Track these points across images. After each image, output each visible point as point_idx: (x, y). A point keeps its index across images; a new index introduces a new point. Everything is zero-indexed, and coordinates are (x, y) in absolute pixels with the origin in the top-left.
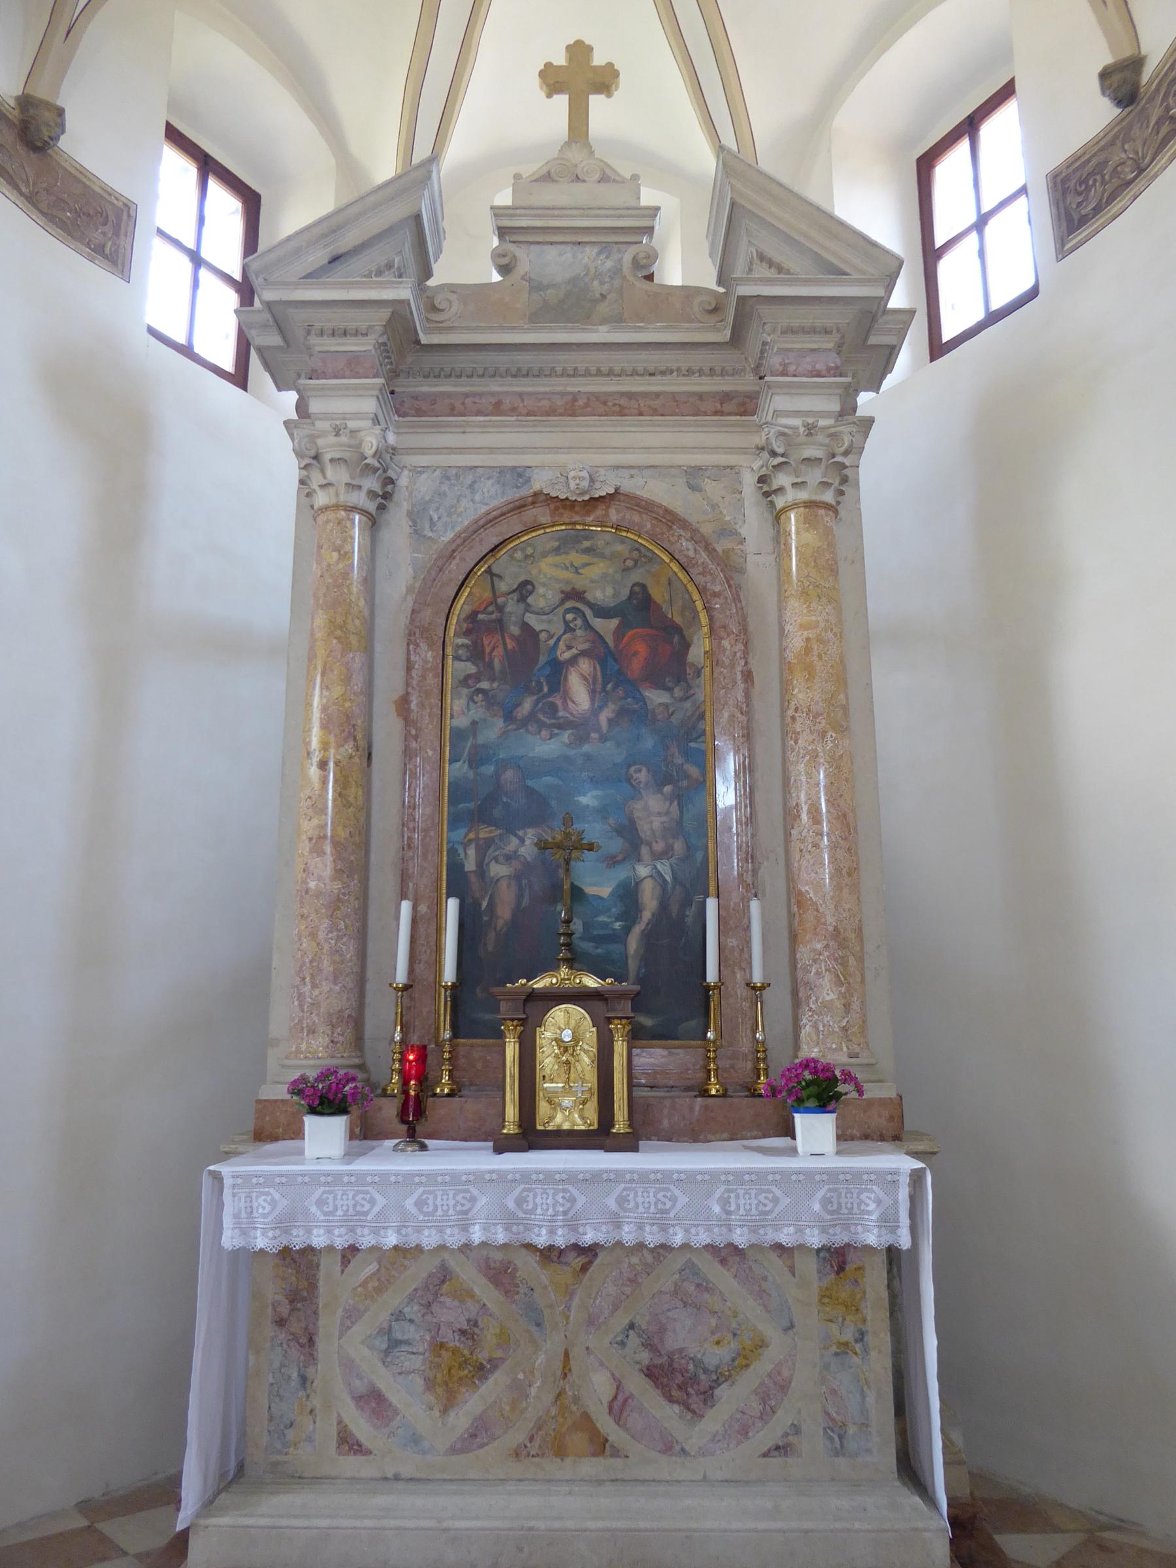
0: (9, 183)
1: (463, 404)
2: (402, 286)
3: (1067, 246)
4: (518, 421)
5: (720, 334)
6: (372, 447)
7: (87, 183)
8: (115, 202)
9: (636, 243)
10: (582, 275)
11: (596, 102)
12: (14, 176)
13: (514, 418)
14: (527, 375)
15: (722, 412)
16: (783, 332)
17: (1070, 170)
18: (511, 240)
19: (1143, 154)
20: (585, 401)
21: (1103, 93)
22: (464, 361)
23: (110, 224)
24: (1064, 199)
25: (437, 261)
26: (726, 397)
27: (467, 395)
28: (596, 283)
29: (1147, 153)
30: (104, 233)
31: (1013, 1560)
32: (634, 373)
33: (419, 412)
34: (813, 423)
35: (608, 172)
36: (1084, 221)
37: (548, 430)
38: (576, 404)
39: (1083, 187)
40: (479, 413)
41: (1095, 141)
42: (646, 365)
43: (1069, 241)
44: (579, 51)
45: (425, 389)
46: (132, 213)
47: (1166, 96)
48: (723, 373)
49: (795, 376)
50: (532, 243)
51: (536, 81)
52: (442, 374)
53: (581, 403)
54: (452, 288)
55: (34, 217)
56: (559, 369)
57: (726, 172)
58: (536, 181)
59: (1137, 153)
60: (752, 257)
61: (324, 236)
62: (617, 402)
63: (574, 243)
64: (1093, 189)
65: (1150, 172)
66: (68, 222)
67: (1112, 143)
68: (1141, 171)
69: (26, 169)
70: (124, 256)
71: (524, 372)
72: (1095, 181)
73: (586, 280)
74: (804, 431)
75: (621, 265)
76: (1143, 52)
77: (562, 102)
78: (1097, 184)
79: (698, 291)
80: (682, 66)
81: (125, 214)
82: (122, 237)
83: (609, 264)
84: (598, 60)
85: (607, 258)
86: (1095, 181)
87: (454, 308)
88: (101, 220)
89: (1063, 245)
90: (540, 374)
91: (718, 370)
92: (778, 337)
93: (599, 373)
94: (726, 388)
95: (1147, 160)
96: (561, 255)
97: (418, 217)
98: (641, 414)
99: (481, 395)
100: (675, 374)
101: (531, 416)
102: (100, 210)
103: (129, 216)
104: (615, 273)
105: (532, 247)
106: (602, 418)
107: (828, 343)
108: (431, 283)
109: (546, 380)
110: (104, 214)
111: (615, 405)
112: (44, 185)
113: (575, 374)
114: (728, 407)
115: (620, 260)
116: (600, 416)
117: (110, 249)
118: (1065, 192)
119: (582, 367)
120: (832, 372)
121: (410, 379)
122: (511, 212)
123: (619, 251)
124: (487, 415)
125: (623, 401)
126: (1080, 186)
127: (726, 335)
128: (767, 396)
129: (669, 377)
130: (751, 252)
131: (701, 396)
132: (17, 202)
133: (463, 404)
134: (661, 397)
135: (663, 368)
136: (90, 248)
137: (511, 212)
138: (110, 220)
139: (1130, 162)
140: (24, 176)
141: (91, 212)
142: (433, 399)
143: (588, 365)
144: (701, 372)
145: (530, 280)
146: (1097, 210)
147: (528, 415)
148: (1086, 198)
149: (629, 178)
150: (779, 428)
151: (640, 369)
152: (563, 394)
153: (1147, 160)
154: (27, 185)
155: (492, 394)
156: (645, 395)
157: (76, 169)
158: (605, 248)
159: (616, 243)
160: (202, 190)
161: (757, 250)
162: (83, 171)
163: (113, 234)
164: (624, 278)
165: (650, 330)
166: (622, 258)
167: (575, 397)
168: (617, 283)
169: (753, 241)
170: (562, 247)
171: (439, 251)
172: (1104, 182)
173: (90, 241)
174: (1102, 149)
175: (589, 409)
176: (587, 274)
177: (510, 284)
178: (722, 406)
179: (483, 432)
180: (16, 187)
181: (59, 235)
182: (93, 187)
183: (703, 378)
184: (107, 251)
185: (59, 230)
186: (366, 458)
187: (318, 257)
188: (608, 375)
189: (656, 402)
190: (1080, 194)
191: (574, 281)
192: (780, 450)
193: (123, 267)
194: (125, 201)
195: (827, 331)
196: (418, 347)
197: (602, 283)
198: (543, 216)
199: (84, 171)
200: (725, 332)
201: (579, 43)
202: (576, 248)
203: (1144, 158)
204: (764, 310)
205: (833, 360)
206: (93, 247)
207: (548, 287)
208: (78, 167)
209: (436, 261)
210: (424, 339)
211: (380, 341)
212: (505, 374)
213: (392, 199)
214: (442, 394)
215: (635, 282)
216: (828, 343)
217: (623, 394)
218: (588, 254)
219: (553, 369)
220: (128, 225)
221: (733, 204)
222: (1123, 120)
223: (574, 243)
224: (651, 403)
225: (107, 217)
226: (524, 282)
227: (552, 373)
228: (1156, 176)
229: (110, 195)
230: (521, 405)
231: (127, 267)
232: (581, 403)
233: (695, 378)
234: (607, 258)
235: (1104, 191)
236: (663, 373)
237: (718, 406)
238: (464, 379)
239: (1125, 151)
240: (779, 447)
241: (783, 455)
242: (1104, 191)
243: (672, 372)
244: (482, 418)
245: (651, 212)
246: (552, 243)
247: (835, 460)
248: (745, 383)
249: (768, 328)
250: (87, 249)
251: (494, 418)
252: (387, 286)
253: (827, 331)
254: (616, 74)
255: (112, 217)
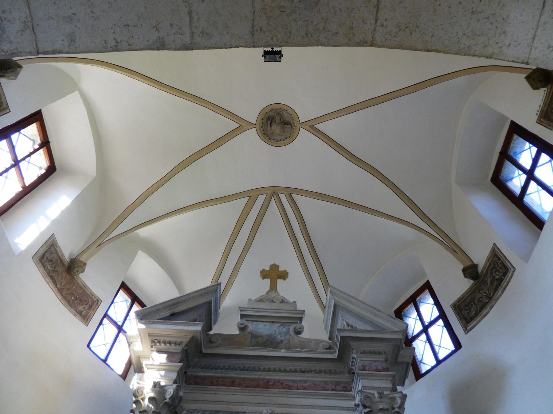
0: (53, 282)
1: (217, 381)
2: (198, 325)
3: (468, 328)
4: (242, 389)
5: (333, 355)
6: (170, 394)
7: (86, 290)
8: (94, 298)
9: (295, 323)
10: (273, 333)
11: (279, 281)
12: (56, 281)
13: (240, 388)
14: (247, 370)
15: (336, 390)
16: (362, 353)
17: (460, 303)
18: (246, 319)
19: (489, 293)
20: (273, 382)
21: (465, 277)
22: (220, 362)
23: (89, 305)
24: (461, 313)
25: (214, 324)
26: (337, 383)
27: (219, 377)
28: (279, 336)
29: (491, 292)
30: (84, 308)
31: (16, 60)
32: (296, 371)
33: (196, 383)
34: (382, 392)
35: (284, 300)
36: (472, 319)
37: (255, 395)
38: (269, 383)
39: (467, 307)
40: (224, 385)
41: (467, 292)
42: (300, 368)
43: (468, 326)
44: (274, 267)
45: (201, 374)
46: (99, 303)
47: (491, 274)
48: (335, 373)
49: (369, 371)
50: (253, 321)
51: (259, 274)
52: (210, 368)
53: (271, 383)
54: (219, 335)
55: (58, 296)
56: (262, 368)
57: (331, 294)
58: (257, 301)
59: (487, 293)
60: (344, 325)
61: (171, 306)
62: (287, 383)
63: (270, 322)
64: (472, 308)
65: (495, 297)
66: (71, 301)
67: (474, 291)
68: (490, 299)
69: (63, 280)
70: (89, 317)
71: (246, 368)
72: (472, 305)
73: (275, 335)
74: (378, 396)
75: (289, 331)
76: (475, 263)
77: (267, 281)
78: (473, 306)
79: (322, 341)
80: (308, 279)
81: (96, 303)
82: (91, 310)
83: (284, 330)
84: (281, 269)
85: (283, 327)
86: (472, 305)
87: (219, 342)
88: (86, 303)
89: (466, 328)
90: (254, 370)
91: (333, 372)
92: (360, 355)
93: (280, 371)
94: (337, 380)
95: (492, 294)
96: (265, 326)
97: (210, 303)
98: (298, 389)
99: (226, 378)
100: (313, 372)
101: (248, 387)
102: (86, 299)
103: (97, 304)
104: (286, 333)
105: (253, 322)
106: (281, 390)
107: (382, 358)
108: (211, 333)
109: (256, 373)
110: (87, 301)
111: (286, 385)
112: (68, 287)
113: (269, 370)
114: (338, 388)
115: (289, 329)
116: (280, 389)
117: (84, 313)
118: (460, 310)
119: (272, 368)
120: (386, 370)
121: (195, 369)
122: (246, 309)
123: (288, 326)
124: (228, 386)
125: (290, 384)
126: (466, 307)
127: (335, 356)
128: (357, 380)
129: (311, 374)
130: (344, 324)
131: (326, 383)
132: (53, 289)
133: (217, 381)
134: (307, 382)
135: (308, 370)
136: (76, 311)
137: (246, 309)
138: (89, 303)
139: (484, 296)
140: (61, 282)
141: (82, 300)
142: (204, 378)
143: (274, 367)
144: (326, 372)
145: (252, 334)
146: (477, 314)
147: (246, 387)
148: (470, 311)
149: (292, 302)
150: (366, 394)
151: (298, 370)
152: (263, 380)
153: (492, 294)
154: (61, 285)
155: (232, 378)
156: (300, 381)
157: (83, 285)
158: (283, 324)
159: (287, 323)
160: (132, 304)
161: (346, 322)
162: (85, 286)
163: (88, 309)
164: (290, 335)
165: (302, 352)
166: (290, 328)
167: (268, 381)
168: (288, 337)
169: (343, 319)
170: (266, 323)
171: (216, 321)
172: (475, 305)
173: (77, 309)
174: (471, 294)
175: (275, 386)
176: (275, 333)
177: (243, 335)
178: (336, 387)
179: (225, 394)
180: (56, 285)
181: (65, 304)
182: (87, 291)
183: (326, 375)
184: (83, 314)
185: (66, 303)
186: (166, 399)
187: (167, 313)
188: (283, 371)
189: (306, 384)
190: (467, 310)
191: (269, 336)
192: (367, 405)
193: (87, 321)
194: (98, 298)
195: (380, 353)
196: (201, 354)
197: (281, 336)
198: (258, 311)
199: (86, 286)
200: (335, 354)
201: (274, 265)
202: (271, 324)
203: (490, 294)
204: (353, 344)
205: (385, 365)
206: (77, 311)
207: (259, 337)
208: (84, 284)
209: (214, 324)
210: (204, 351)
211: (185, 348)
212: (237, 369)
213: (201, 296)
214: (208, 377)
215: (295, 337)
216: (382, 358)
217: (290, 381)
218: (276, 327)
219: (259, 368)
220: (95, 307)
221: (335, 306)
222: (476, 284)
223: (270, 322)
224: (303, 385)
225: (88, 302)
226: (249, 335)
227: (259, 370)
228: (498, 299)
229: (93, 295)
230: (244, 383)
231: (89, 320)
232: (271, 383)
233: (323, 375)
234: (283, 327)
235: (477, 308)
236: (308, 372)
237: (334, 388)
238: (219, 370)
239: (481, 293)
240: (367, 403)
241: (369, 407)
242: (477, 308)
243: (312, 371)
244: (225, 387)
245: (301, 312)
246: (261, 322)
247: (394, 411)
248: (345, 378)
249: (354, 351)
250: (75, 311)
251: (230, 388)
252: (192, 325)
253: (380, 353)
254: (287, 273)
255: (90, 303)
